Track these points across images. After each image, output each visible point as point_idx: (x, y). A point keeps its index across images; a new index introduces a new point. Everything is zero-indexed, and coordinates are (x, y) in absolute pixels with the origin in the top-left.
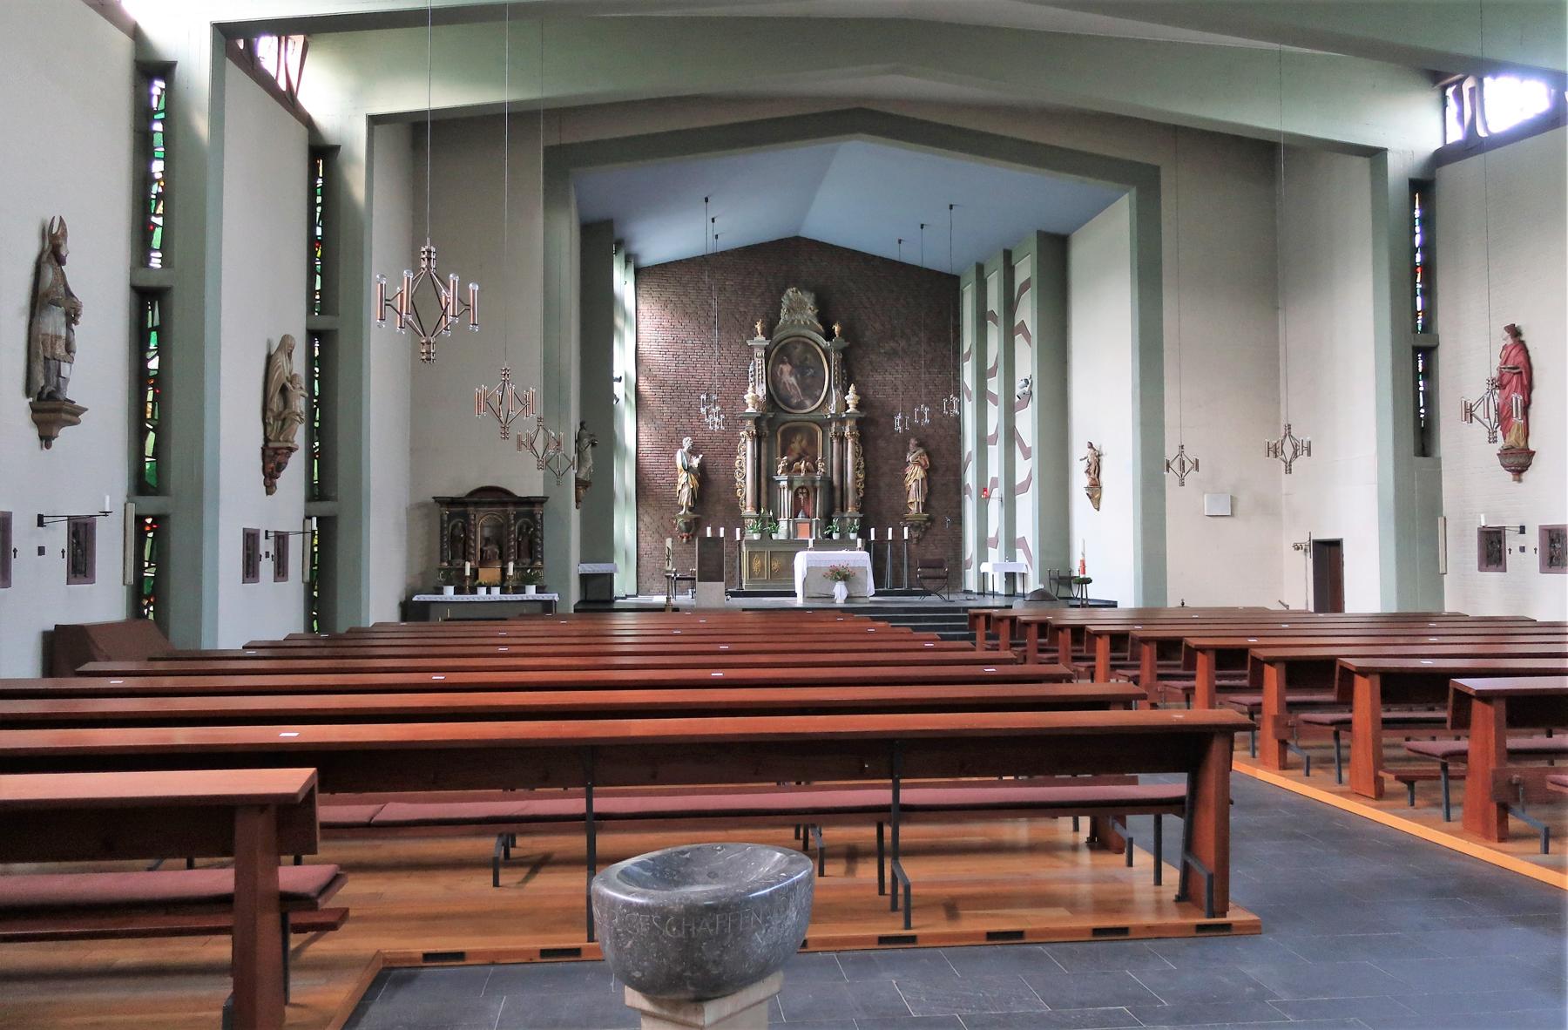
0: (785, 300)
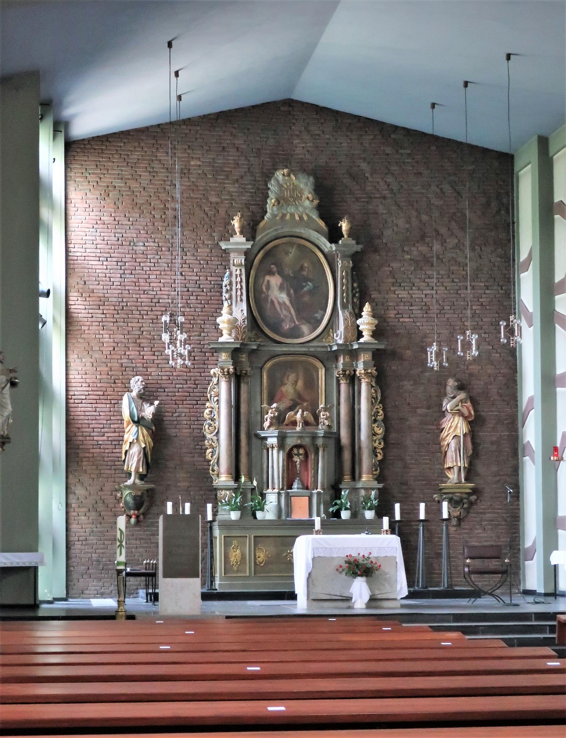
0: (273, 186)
